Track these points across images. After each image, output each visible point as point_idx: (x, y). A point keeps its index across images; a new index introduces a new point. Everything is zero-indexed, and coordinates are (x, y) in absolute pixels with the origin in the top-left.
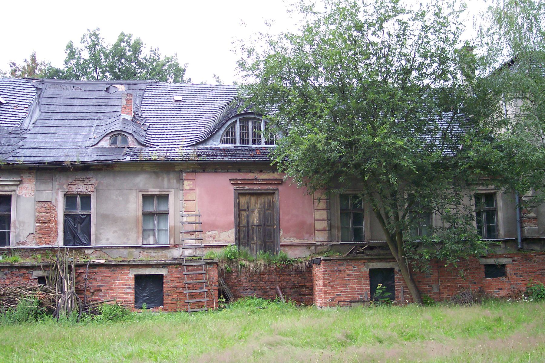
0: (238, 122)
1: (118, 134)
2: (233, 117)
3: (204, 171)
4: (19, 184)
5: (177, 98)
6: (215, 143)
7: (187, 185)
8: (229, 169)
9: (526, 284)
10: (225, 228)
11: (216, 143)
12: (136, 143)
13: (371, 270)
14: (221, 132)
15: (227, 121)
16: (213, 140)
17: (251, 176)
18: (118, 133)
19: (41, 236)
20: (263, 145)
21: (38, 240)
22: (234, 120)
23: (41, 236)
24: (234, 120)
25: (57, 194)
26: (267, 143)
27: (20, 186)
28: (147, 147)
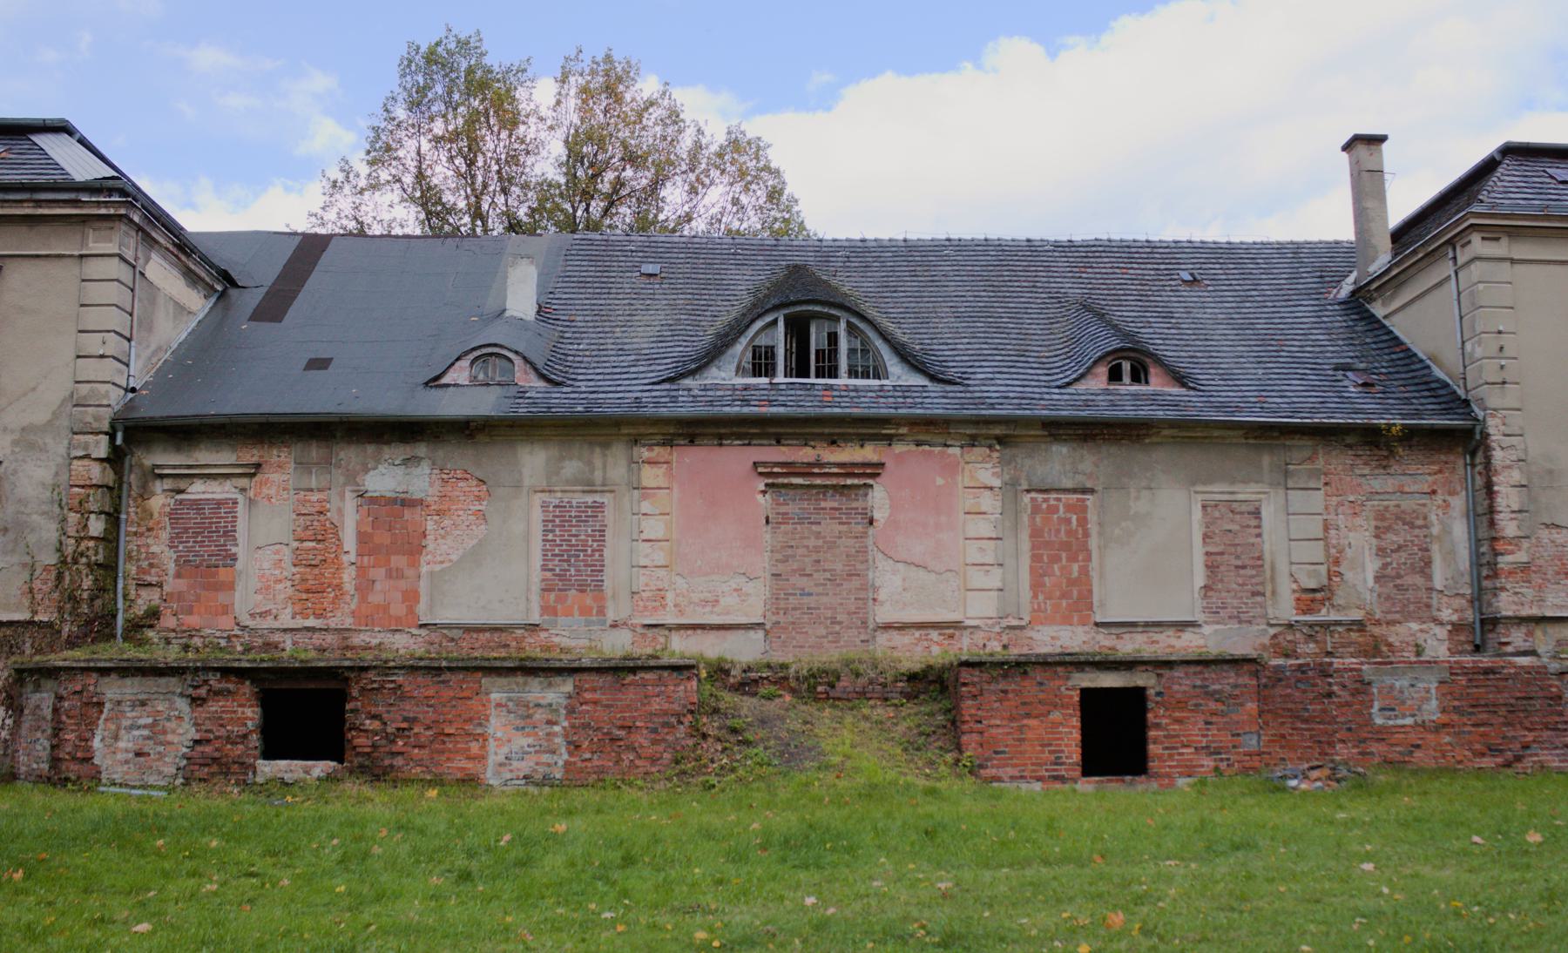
0: (781, 324)
1: (491, 354)
2: (767, 312)
3: (692, 442)
4: (254, 475)
5: (650, 269)
6: (723, 374)
7: (1320, 463)
8: (721, 437)
9: (1484, 735)
10: (314, 587)
11: (726, 375)
12: (532, 376)
13: (1085, 692)
14: (739, 348)
15: (753, 321)
16: (719, 368)
17: (805, 454)
18: (490, 350)
19: (304, 596)
20: (812, 380)
21: (297, 609)
22: (769, 318)
23: (304, 596)
24: (769, 318)
25: (342, 497)
26: (853, 373)
27: (256, 479)
28: (663, 381)
